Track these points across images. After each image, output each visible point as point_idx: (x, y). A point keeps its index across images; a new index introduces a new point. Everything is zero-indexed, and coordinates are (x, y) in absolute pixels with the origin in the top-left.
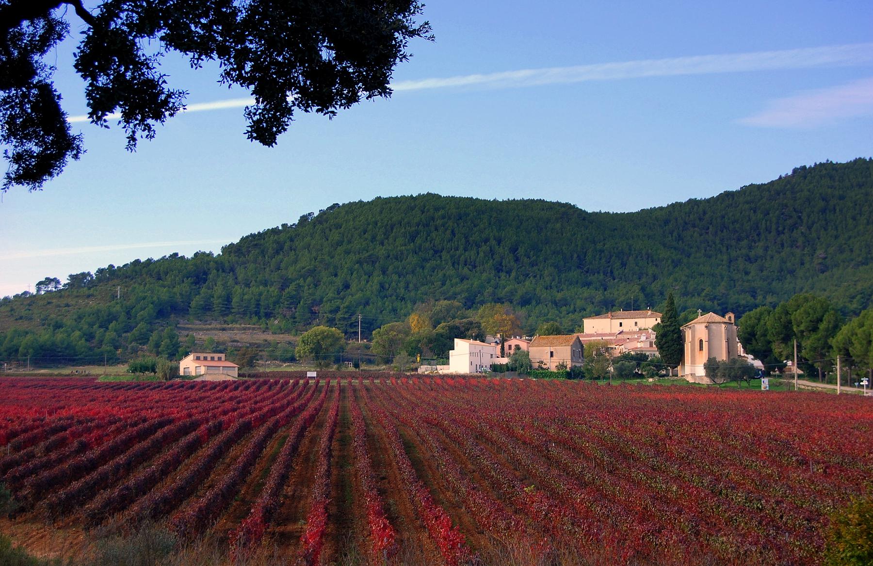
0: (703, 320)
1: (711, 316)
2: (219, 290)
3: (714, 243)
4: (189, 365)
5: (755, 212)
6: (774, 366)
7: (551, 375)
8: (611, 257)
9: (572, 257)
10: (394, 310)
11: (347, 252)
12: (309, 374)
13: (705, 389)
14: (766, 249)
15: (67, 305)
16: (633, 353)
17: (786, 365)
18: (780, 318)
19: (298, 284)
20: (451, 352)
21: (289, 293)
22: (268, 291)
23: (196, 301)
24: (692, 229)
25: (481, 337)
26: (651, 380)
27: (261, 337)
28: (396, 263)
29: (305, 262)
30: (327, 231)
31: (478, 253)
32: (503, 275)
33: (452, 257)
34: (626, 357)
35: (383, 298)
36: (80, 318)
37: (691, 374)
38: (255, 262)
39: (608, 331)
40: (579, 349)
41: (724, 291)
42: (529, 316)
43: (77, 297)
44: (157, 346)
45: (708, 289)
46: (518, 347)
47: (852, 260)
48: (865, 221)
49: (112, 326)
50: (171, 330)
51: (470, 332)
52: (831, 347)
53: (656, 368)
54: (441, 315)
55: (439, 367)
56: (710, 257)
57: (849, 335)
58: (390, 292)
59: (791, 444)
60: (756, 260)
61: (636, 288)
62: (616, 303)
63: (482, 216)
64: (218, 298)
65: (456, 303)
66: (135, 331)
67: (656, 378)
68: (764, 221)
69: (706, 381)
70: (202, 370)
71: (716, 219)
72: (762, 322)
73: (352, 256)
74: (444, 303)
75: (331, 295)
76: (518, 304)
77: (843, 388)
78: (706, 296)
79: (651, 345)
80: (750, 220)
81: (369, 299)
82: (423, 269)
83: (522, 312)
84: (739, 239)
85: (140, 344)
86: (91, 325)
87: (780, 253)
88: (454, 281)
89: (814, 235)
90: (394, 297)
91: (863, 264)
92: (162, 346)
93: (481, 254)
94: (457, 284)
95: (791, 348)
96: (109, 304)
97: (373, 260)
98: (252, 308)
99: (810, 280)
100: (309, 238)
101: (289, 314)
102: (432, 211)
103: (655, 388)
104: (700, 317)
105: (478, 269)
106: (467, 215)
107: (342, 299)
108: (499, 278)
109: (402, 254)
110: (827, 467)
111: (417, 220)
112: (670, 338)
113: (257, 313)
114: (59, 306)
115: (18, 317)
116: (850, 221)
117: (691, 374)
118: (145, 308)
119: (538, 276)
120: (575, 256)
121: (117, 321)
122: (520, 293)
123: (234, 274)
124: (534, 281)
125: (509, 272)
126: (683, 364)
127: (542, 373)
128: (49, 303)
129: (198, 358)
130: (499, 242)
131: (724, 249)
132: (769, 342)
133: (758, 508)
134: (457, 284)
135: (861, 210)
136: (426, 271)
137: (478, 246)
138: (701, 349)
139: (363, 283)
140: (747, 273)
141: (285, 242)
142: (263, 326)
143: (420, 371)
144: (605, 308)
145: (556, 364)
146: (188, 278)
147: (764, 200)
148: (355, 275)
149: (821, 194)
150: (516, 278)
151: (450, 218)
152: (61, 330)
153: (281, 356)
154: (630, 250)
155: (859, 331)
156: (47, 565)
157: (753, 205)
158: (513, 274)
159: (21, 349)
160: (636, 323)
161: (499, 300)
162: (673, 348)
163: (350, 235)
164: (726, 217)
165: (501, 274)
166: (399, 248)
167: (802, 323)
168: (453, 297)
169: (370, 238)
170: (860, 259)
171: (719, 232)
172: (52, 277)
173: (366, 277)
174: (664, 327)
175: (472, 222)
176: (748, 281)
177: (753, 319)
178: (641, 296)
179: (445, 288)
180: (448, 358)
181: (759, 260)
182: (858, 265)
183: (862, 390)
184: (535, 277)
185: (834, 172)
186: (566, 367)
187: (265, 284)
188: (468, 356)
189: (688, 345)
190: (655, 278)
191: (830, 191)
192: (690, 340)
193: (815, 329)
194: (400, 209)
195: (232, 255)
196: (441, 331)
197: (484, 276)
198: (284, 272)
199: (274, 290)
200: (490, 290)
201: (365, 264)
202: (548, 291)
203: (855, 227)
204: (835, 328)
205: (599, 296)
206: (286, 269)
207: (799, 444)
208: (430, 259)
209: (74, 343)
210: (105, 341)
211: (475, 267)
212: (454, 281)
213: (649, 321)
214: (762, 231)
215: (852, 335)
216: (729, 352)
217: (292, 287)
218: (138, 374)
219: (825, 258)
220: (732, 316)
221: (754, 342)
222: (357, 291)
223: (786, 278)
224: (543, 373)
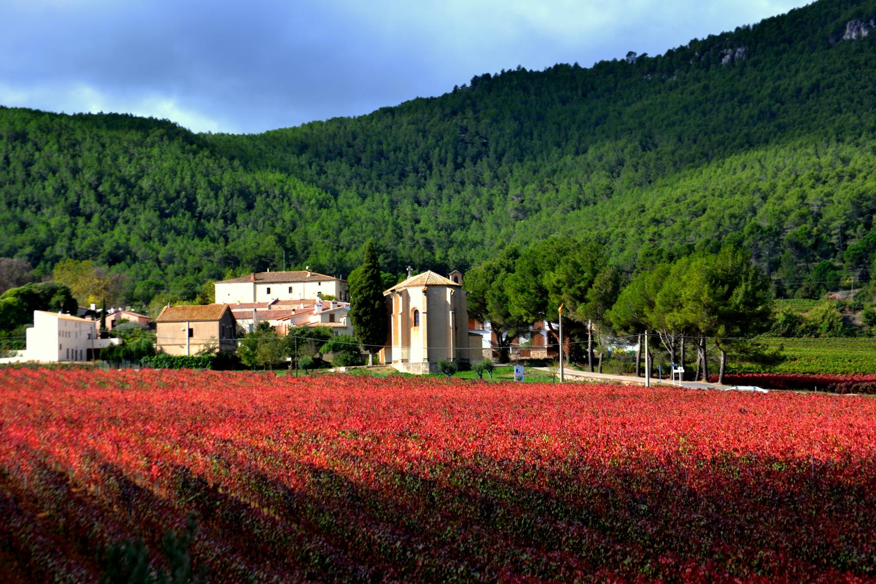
0: (419, 282)
14: (440, 188)
37: (403, 361)
48: (574, 149)
61: (271, 239)
68: (438, 149)
122: (107, 247)
125: (89, 218)
137: (44, 178)
158: (96, 219)
189: (396, 318)
192: (401, 310)
216: (456, 328)
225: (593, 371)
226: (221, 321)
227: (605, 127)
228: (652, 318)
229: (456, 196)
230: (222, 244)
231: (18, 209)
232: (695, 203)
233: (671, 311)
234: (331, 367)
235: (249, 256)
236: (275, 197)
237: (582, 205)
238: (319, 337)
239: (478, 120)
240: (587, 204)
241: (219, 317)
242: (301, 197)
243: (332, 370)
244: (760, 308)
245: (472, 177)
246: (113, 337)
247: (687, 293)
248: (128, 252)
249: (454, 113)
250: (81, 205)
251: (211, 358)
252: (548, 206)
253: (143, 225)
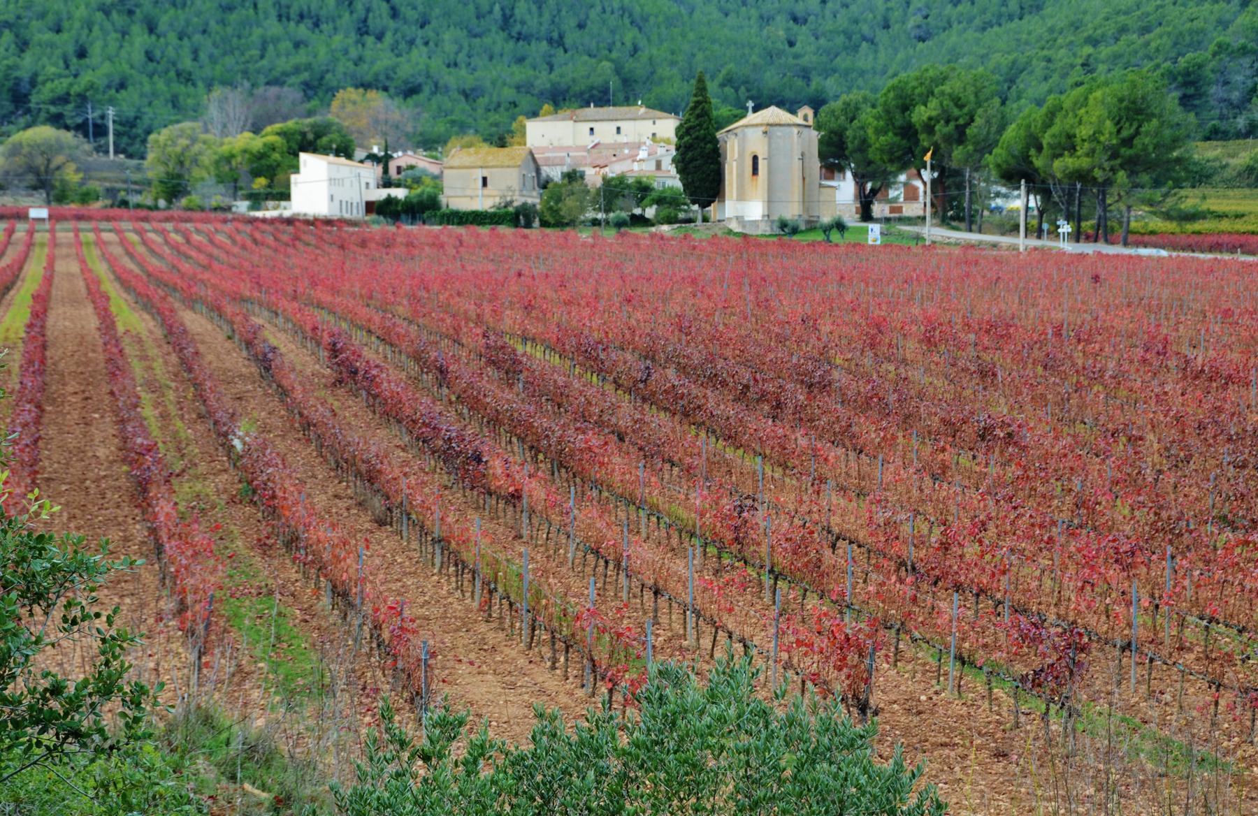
1: (774, 113)
12: (34, 213)
20: (293, 177)
25: (345, 151)
32: (370, 40)
39: (570, 143)
108: (363, 45)
117: (737, 218)
125: (380, 37)
126: (723, 200)
138: (755, 171)
156: (156, 3)
158: (388, 38)
184: (426, 44)
188: (325, 185)
192: (736, 156)
196: (272, 139)
225: (970, 230)
228: (1038, 162)
229: (843, 11)
230: (544, 73)
231: (292, 24)
232: (1148, 14)
233: (1061, 155)
234: (653, 225)
236: (612, 12)
237: (1003, 21)
238: (643, 191)
240: (1011, 18)
243: (653, 229)
244: (1175, 154)
246: (398, 185)
247: (1084, 132)
250: (370, 21)
251: (507, 214)
252: (960, 22)
253: (449, 48)
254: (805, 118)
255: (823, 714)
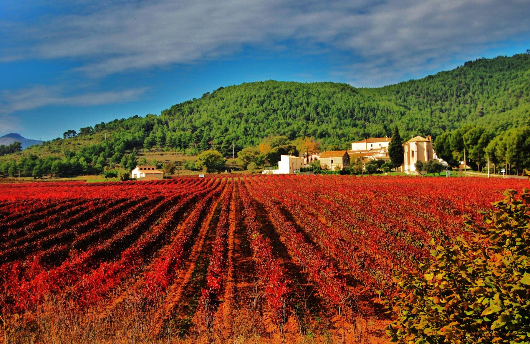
0: (414, 140)
2: (159, 134)
3: (423, 103)
4: (137, 173)
5: (445, 86)
6: (454, 164)
7: (332, 172)
8: (368, 111)
9: (347, 111)
10: (252, 142)
11: (227, 112)
13: (414, 177)
14: (451, 105)
15: (79, 144)
16: (376, 160)
17: (460, 164)
18: (456, 138)
19: (201, 130)
20: (279, 162)
21: (196, 134)
22: (185, 134)
23: (147, 140)
24: (411, 96)
25: (296, 154)
26: (386, 174)
27: (180, 159)
28: (253, 117)
29: (205, 118)
30: (217, 101)
31: (297, 111)
33: (283, 113)
34: (373, 162)
35: (246, 136)
36: (85, 150)
38: (179, 118)
39: (365, 149)
40: (346, 159)
41: (428, 128)
42: (324, 143)
43: (84, 139)
44: (125, 163)
45: (420, 127)
46: (316, 159)
47: (497, 110)
48: (503, 89)
49: (102, 154)
50: (133, 156)
51: (290, 151)
52: (484, 153)
53: (390, 168)
54: (276, 143)
55: (273, 170)
56: (421, 110)
57: (494, 145)
58: (250, 133)
59: (451, 202)
60: (446, 111)
62: (371, 135)
63: (299, 91)
64: (159, 138)
65: (285, 137)
66: (114, 157)
67: (389, 172)
68: (449, 91)
69: (416, 173)
70: (144, 175)
71: (424, 90)
72: (447, 140)
73: (229, 114)
74: (278, 137)
75: (218, 135)
76: (318, 137)
77: (491, 175)
78: (419, 130)
79: (387, 156)
80: (442, 90)
81: (239, 136)
82: (268, 120)
83: (320, 141)
84: (436, 101)
85: (116, 163)
86: (90, 154)
87: (458, 107)
88: (284, 126)
89: (476, 97)
90: (252, 135)
91: (502, 111)
92: (128, 164)
93: (299, 111)
94: (286, 127)
95: (462, 154)
96: (101, 143)
97: (240, 116)
98: (177, 142)
99: (475, 121)
100: (207, 105)
101: (196, 145)
102: (272, 89)
103: (387, 177)
104: (412, 139)
105: (297, 119)
106: (291, 91)
107: (225, 137)
109: (256, 112)
110: (473, 216)
111: (264, 94)
112: (396, 150)
113: (180, 146)
114: (74, 145)
115: (53, 151)
116: (495, 89)
118: (119, 145)
119: (329, 122)
120: (349, 111)
121: (104, 151)
122: (319, 132)
123: (168, 126)
124: (327, 125)
125: (313, 121)
126: (404, 165)
127: (327, 172)
128: (69, 143)
129: (141, 169)
130: (308, 104)
131: (428, 106)
132: (451, 151)
133: (420, 245)
134: (286, 127)
135: (501, 83)
136: (269, 121)
137: (297, 107)
139: (236, 128)
140: (441, 118)
141: (194, 108)
142: (183, 152)
143: (263, 173)
144: (366, 137)
145: (334, 167)
146: (142, 128)
147: (450, 79)
148: (231, 124)
149: (480, 76)
150: (318, 123)
151: (281, 93)
152: (74, 157)
153: (191, 167)
154: (378, 107)
155: (500, 143)
157: (444, 82)
158: (316, 121)
159: (52, 167)
160: (380, 145)
161: (309, 136)
162: (398, 156)
163: (228, 103)
164: (429, 89)
165: (309, 122)
166: (255, 109)
167: (468, 140)
168: (284, 134)
169: (239, 104)
170: (501, 109)
171: (426, 97)
172: (71, 130)
173: (237, 125)
174: (392, 144)
175: (293, 95)
176: (442, 122)
177: (442, 139)
178: (384, 131)
179: (279, 129)
180: (278, 166)
181: (447, 111)
182: (499, 112)
183: (502, 175)
185: (486, 64)
186: (340, 168)
187: (184, 130)
190: (391, 121)
191: (484, 73)
192: (407, 151)
193: (476, 143)
194: (255, 88)
195: (167, 115)
197: (300, 123)
198: (194, 123)
199: (188, 133)
200: (303, 130)
201: (237, 118)
202: (335, 130)
203: (498, 92)
204: (485, 144)
205: (361, 132)
206: (195, 122)
207: (457, 202)
208: (271, 115)
209: (81, 163)
210: (98, 162)
211: (295, 118)
212: (284, 126)
213: (385, 144)
214: (448, 96)
215: (496, 145)
217: (198, 131)
218: (109, 178)
219: (482, 109)
220: (430, 138)
221: (443, 152)
222: (232, 132)
223: (461, 120)
224: (326, 171)
226: (343, 157)
227: (516, 80)
235: (374, 133)
239: (466, 78)
241: (343, 155)
242: (275, 114)
245: (463, 101)
248: (327, 133)
249: (457, 76)
254: (429, 139)
255: (472, 256)
